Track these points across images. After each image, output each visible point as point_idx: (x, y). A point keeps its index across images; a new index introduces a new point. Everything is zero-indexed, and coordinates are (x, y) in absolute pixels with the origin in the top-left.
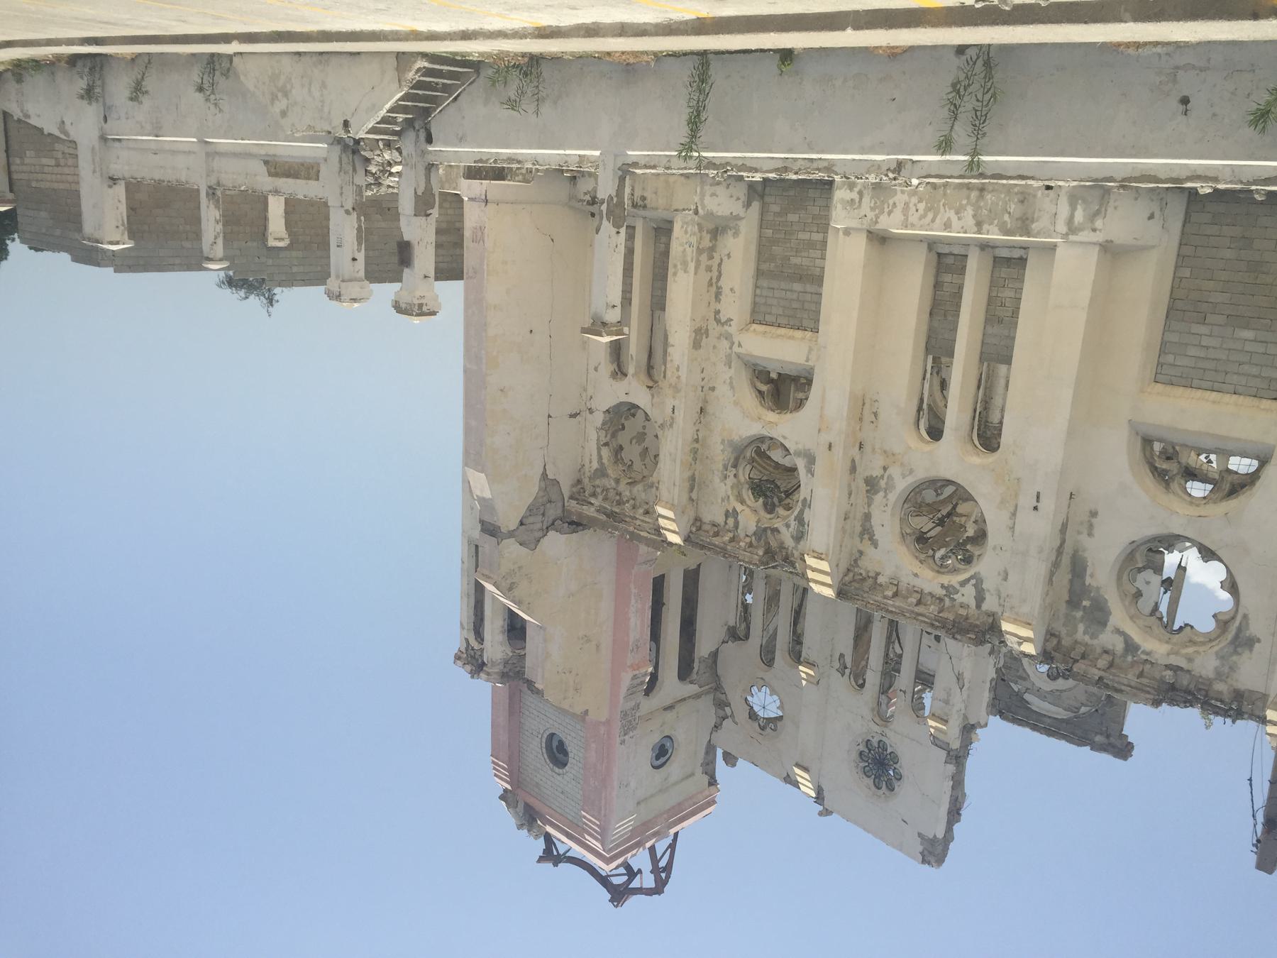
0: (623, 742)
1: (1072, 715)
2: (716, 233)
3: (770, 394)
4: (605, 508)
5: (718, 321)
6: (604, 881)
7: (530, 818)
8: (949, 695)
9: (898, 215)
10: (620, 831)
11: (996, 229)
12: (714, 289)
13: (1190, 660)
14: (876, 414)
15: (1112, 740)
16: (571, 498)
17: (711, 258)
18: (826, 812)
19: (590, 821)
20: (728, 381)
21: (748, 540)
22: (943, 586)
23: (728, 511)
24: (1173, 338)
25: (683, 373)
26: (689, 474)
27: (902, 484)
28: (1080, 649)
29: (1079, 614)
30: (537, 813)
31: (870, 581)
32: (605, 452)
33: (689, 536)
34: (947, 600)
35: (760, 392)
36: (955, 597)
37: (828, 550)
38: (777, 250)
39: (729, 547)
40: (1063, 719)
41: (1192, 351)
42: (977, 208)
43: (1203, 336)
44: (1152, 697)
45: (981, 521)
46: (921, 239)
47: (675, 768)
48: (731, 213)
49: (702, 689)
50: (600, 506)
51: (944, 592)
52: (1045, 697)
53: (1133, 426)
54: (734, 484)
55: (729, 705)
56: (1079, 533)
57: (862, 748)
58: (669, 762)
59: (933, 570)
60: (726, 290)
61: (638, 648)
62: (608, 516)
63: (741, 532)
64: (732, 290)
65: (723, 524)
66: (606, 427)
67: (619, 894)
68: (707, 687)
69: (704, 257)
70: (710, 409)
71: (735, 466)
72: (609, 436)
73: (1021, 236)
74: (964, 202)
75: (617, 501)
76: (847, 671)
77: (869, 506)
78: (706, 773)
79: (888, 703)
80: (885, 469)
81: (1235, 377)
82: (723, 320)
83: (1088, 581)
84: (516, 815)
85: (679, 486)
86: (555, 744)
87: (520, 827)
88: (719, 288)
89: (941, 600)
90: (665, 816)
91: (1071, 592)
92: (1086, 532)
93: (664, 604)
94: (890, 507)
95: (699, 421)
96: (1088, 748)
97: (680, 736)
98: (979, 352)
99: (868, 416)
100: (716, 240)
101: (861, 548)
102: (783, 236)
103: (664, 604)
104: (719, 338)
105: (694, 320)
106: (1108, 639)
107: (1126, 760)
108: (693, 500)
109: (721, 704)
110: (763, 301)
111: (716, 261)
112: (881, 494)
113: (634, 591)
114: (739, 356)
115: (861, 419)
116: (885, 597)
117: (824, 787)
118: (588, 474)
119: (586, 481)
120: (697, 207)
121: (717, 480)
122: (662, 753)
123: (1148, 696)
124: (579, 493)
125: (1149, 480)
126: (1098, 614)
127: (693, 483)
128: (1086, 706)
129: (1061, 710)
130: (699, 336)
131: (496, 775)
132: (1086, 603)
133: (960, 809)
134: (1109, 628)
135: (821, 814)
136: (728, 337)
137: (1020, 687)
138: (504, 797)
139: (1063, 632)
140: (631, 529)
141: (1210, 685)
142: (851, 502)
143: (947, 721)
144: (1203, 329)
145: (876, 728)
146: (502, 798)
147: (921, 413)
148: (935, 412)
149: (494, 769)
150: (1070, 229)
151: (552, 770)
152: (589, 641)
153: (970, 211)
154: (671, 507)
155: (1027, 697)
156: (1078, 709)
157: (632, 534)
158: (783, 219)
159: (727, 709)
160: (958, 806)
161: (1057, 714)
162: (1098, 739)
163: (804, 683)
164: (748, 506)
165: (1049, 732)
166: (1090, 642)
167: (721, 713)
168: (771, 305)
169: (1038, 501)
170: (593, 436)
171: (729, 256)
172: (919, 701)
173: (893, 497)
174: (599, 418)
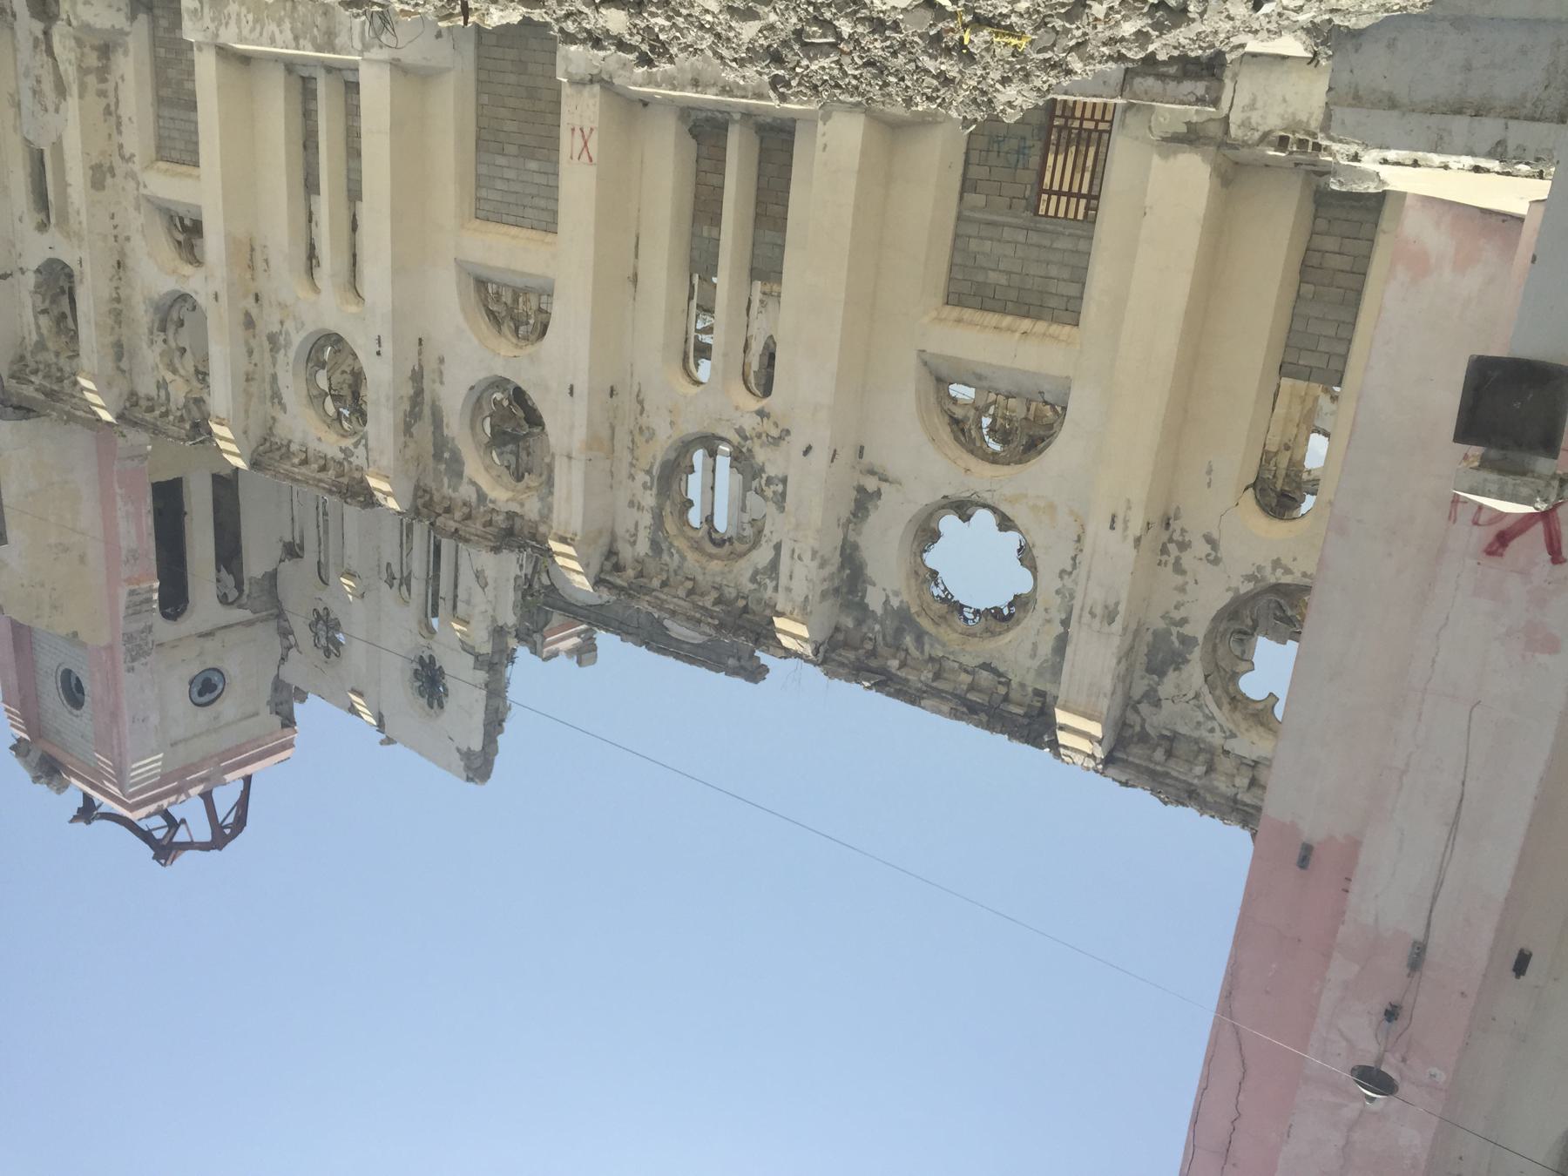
0: (131, 670)
1: (706, 638)
2: (105, 51)
4: (44, 386)
5: (122, 157)
6: (146, 836)
7: (50, 770)
8: (470, 595)
9: (233, 28)
10: (142, 774)
11: (309, 46)
12: (113, 119)
13: (522, 505)
14: (266, 261)
16: (12, 377)
17: (104, 80)
18: (389, 741)
19: (104, 763)
20: (140, 229)
21: (179, 414)
22: (341, 449)
23: (158, 382)
24: (484, 170)
25: (84, 217)
26: (110, 339)
27: (297, 339)
28: (447, 504)
29: (442, 467)
30: (62, 765)
31: (284, 450)
32: (44, 321)
33: (124, 414)
34: (345, 463)
35: (179, 243)
36: (351, 459)
37: (229, 415)
38: (172, 73)
39: (159, 423)
41: (500, 185)
42: (293, 21)
43: (1064, 308)
44: (492, 544)
46: (277, 58)
47: (228, 707)
48: (113, 26)
49: (257, 615)
50: (41, 384)
51: (343, 456)
53: (461, 265)
54: (163, 351)
55: (292, 633)
56: (434, 381)
57: (416, 666)
58: (219, 700)
59: (338, 434)
60: (125, 120)
61: (136, 559)
62: (46, 394)
63: (173, 407)
64: (130, 119)
65: (156, 397)
66: (43, 290)
67: (165, 851)
68: (264, 613)
69: (92, 80)
70: (130, 262)
71: (163, 329)
72: (47, 302)
73: (329, 52)
74: (282, 13)
75: (57, 378)
76: (396, 583)
77: (274, 366)
78: (277, 713)
79: (543, 642)
80: (282, 323)
81: (530, 210)
82: (127, 155)
83: (446, 432)
84: (27, 765)
85: (98, 352)
86: (73, 682)
87: (36, 779)
88: (119, 117)
89: (341, 464)
90: (216, 759)
91: (435, 445)
92: (438, 380)
93: (186, 513)
94: (291, 365)
95: (117, 277)
97: (231, 667)
99: (260, 265)
100: (108, 59)
101: (274, 414)
102: (174, 56)
103: (186, 513)
104: (125, 178)
105: (88, 154)
106: (466, 492)
107: (756, 683)
108: (123, 371)
109: (285, 633)
110: (166, 134)
111: (110, 86)
112: (282, 351)
113: (118, 491)
114: (148, 199)
115: (252, 267)
116: (293, 465)
117: (384, 714)
118: (29, 348)
119: (28, 356)
120: (68, 16)
121: (145, 346)
122: (207, 688)
123: (487, 543)
124: (20, 371)
125: (484, 323)
126: (455, 467)
127: (119, 350)
130: (99, 176)
131: (12, 725)
132: (446, 455)
133: (503, 720)
134: (465, 480)
135: (382, 743)
136: (131, 175)
138: (19, 748)
139: (433, 486)
140: (68, 408)
141: (537, 528)
142: (253, 362)
143: (468, 623)
144: (501, 161)
145: (422, 641)
146: (13, 748)
147: (314, 261)
149: (9, 718)
150: (363, 44)
151: (71, 713)
152: (66, 550)
153: (287, 25)
154: (93, 378)
157: (68, 413)
158: (172, 36)
159: (291, 637)
160: (500, 717)
161: (694, 638)
163: (350, 597)
164: (181, 376)
165: (691, 660)
166: (453, 495)
167: (286, 643)
168: (174, 139)
169: (380, 346)
170: (28, 301)
171: (122, 78)
172: (589, 642)
173: (292, 354)
174: (30, 279)
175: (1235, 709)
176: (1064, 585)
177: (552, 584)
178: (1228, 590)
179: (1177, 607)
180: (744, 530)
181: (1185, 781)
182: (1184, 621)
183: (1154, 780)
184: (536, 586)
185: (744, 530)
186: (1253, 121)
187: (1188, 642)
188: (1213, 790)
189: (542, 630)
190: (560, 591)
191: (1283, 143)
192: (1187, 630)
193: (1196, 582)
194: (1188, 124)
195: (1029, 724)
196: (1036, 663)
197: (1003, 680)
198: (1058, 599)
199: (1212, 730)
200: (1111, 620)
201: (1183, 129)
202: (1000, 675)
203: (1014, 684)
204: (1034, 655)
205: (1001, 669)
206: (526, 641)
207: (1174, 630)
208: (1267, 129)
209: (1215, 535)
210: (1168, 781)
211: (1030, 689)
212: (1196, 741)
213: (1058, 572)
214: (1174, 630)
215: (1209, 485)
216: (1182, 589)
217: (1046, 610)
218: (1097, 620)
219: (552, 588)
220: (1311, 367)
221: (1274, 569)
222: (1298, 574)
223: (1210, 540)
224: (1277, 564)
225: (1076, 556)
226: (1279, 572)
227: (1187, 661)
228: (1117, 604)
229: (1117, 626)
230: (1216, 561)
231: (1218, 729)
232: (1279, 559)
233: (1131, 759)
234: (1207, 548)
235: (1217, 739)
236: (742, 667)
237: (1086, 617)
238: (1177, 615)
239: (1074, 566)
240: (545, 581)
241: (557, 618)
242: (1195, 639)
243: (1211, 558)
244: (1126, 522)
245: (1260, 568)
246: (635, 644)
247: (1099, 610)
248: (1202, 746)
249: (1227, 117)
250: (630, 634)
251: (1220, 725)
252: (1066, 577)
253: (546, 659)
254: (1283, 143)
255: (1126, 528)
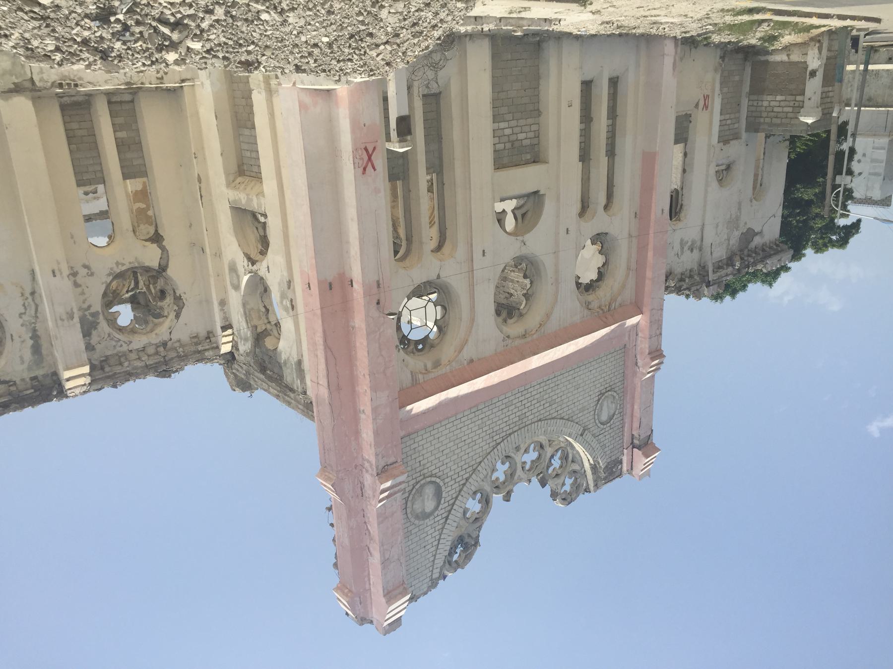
175: (123, 333)
176: (24, 320)
178: (103, 284)
179: (84, 302)
181: (123, 372)
182: (89, 307)
183: (113, 379)
186: (45, 78)
187: (95, 315)
188: (136, 368)
191: (61, 86)
192: (92, 310)
193: (88, 287)
194: (14, 83)
195: (40, 393)
196: (25, 366)
197: (12, 383)
198: (24, 328)
199: (121, 346)
200: (72, 318)
201: (12, 86)
202: (10, 381)
203: (18, 382)
204: (23, 362)
205: (7, 379)
207: (87, 313)
208: (53, 81)
209: (87, 264)
210: (117, 376)
211: (28, 380)
212: (117, 355)
213: (18, 315)
214: (87, 313)
215: (75, 242)
216: (83, 293)
217: (20, 337)
218: (66, 321)
220: (89, 179)
221: (118, 266)
222: (128, 264)
223: (86, 267)
224: (117, 264)
225: (24, 303)
226: (120, 266)
227: (99, 323)
228: (72, 309)
229: (76, 319)
230: (92, 274)
231: (123, 344)
232: (117, 262)
233: (97, 377)
234: (86, 270)
235: (125, 348)
237: (59, 322)
238: (85, 306)
239: (25, 309)
242: (98, 312)
243: (90, 273)
244: (60, 270)
245: (111, 269)
247: (64, 317)
248: (120, 355)
249: (32, 79)
251: (124, 342)
252: (23, 316)
254: (61, 86)
255: (61, 274)
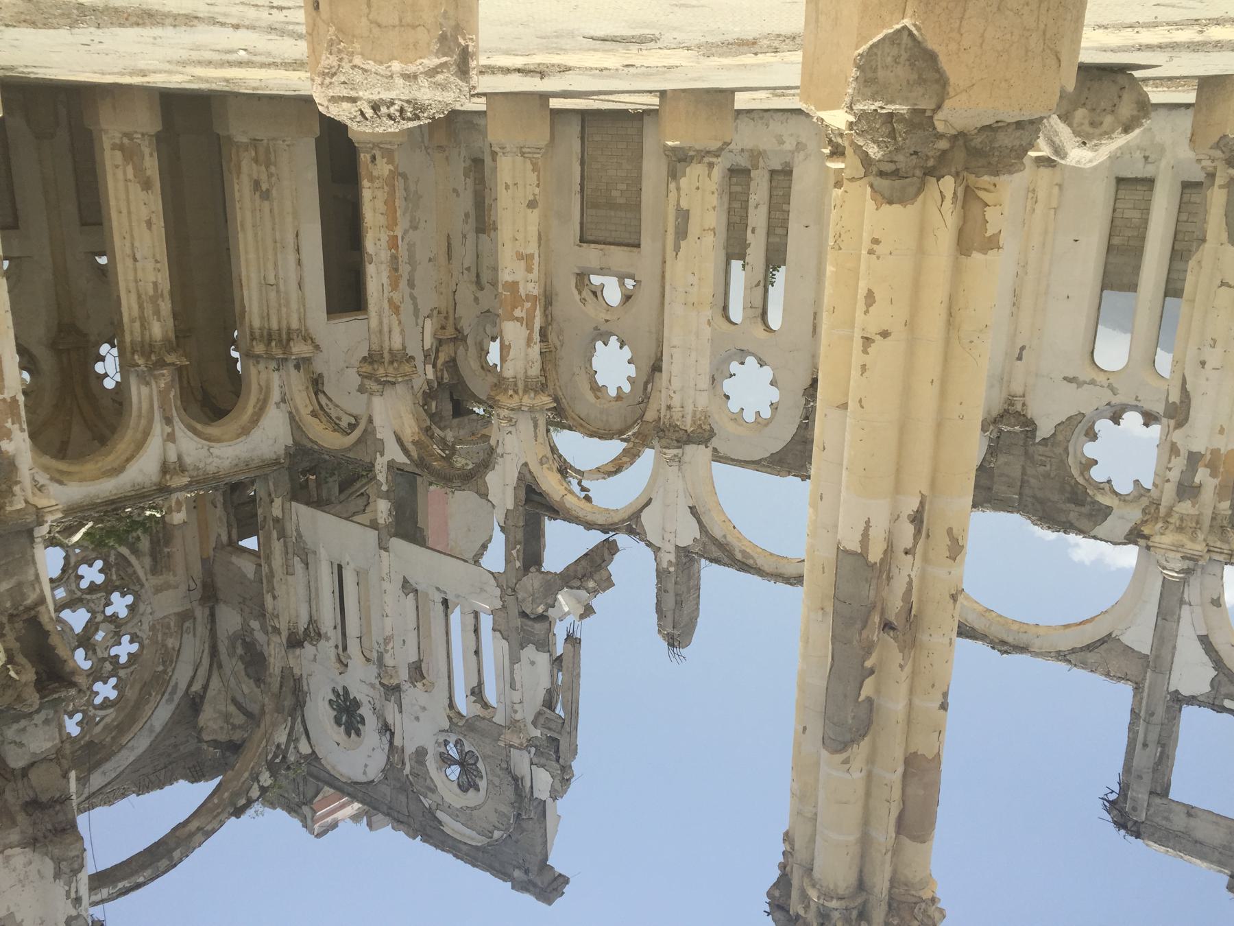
3: (182, 410)
15: (531, 876)
40: (477, 846)
43: (1119, 197)
45: (984, 430)
52: (457, 816)
96: (509, 884)
98: (1110, 218)
128: (499, 829)
129: (474, 834)
137: (430, 802)
148: (297, 422)
155: (439, 814)
156: (492, 832)
161: (472, 839)
162: (517, 873)
177: (314, 752)
180: (515, 712)
184: (292, 758)
185: (515, 712)
189: (311, 801)
190: (323, 762)
206: (296, 812)
219: (314, 757)
236: (530, 881)
240: (304, 748)
241: (327, 790)
246: (407, 834)
250: (402, 822)
253: (319, 836)
